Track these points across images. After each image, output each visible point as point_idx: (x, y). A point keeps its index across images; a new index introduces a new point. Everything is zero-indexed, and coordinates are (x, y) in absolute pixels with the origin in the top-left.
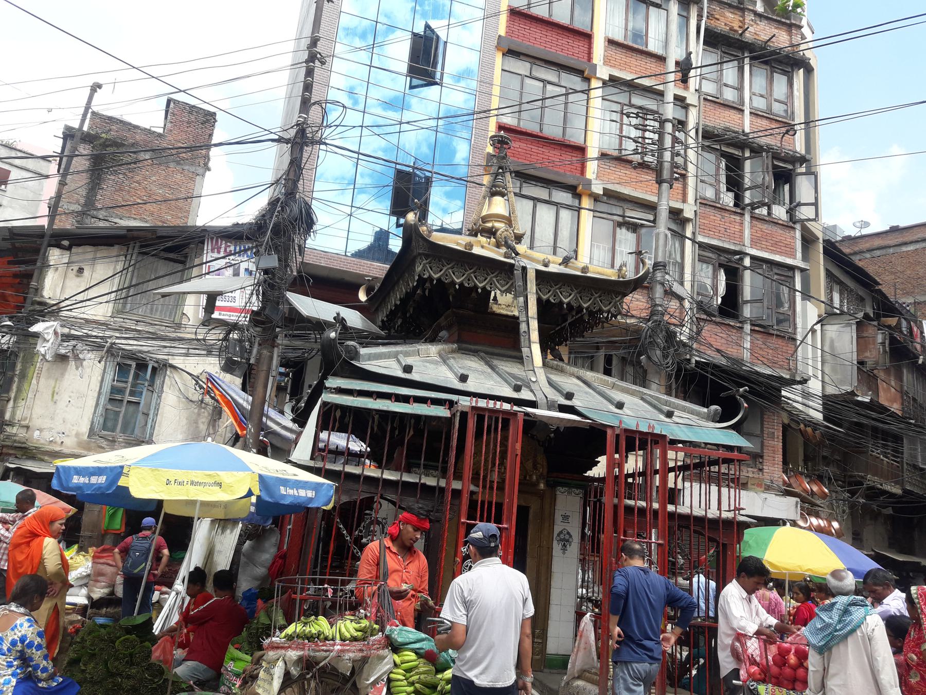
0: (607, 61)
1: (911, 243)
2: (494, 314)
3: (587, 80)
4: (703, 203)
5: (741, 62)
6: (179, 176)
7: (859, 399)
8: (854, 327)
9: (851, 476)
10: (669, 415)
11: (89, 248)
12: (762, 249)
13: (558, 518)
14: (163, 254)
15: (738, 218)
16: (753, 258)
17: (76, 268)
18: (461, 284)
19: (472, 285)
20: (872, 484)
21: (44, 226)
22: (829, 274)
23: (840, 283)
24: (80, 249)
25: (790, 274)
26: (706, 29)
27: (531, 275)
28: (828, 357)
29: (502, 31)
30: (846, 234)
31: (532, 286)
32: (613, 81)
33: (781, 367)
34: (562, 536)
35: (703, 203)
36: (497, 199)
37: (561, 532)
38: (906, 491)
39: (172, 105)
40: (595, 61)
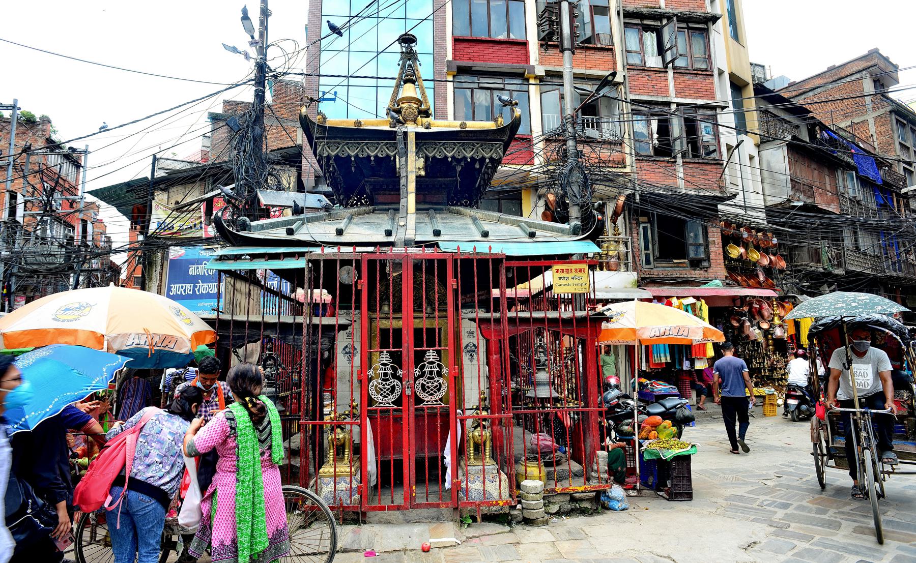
1: (847, 76)
4: (631, 68)
8: (785, 148)
9: (796, 266)
10: (532, 235)
11: (180, 188)
12: (686, 97)
14: (197, 172)
15: (662, 75)
16: (678, 104)
18: (356, 156)
19: (365, 155)
21: (147, 178)
24: (175, 189)
25: (713, 112)
27: (412, 139)
28: (766, 174)
33: (715, 190)
34: (469, 348)
35: (631, 68)
36: (409, 86)
37: (468, 345)
38: (848, 272)
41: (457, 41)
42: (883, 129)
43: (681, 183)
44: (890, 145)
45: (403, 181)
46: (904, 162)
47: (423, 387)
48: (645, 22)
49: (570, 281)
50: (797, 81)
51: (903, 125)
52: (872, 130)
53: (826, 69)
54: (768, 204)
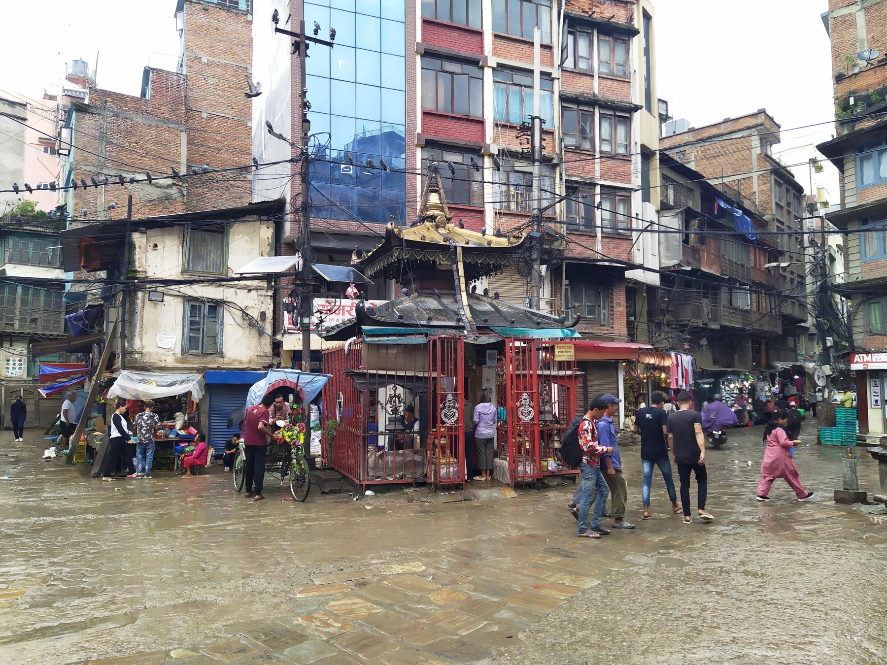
0: (495, 52)
1: (739, 130)
2: (439, 270)
3: (482, 68)
5: (590, 36)
6: (167, 134)
7: (684, 268)
9: (682, 321)
13: (484, 381)
16: (602, 186)
17: (152, 245)
18: (421, 260)
20: (695, 324)
22: (664, 177)
23: (673, 181)
25: (628, 194)
26: (564, 15)
27: (459, 250)
29: (419, 39)
30: (691, 126)
31: (460, 257)
32: (501, 67)
38: (722, 326)
39: (151, 75)
40: (486, 53)
41: (425, 114)
42: (764, 187)
43: (599, 248)
44: (768, 203)
45: (456, 282)
46: (778, 221)
47: (446, 415)
48: (581, 108)
49: (564, 354)
50: (697, 127)
51: (780, 185)
52: (755, 188)
53: (722, 120)
54: (663, 266)
